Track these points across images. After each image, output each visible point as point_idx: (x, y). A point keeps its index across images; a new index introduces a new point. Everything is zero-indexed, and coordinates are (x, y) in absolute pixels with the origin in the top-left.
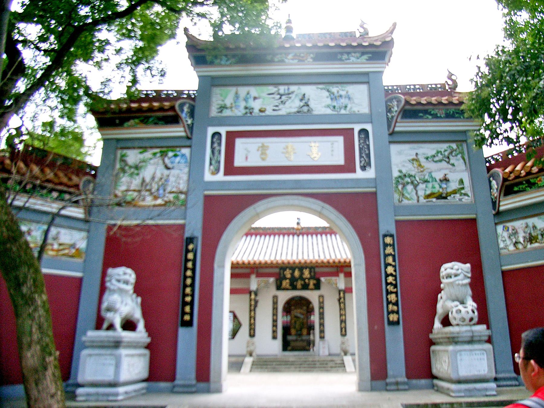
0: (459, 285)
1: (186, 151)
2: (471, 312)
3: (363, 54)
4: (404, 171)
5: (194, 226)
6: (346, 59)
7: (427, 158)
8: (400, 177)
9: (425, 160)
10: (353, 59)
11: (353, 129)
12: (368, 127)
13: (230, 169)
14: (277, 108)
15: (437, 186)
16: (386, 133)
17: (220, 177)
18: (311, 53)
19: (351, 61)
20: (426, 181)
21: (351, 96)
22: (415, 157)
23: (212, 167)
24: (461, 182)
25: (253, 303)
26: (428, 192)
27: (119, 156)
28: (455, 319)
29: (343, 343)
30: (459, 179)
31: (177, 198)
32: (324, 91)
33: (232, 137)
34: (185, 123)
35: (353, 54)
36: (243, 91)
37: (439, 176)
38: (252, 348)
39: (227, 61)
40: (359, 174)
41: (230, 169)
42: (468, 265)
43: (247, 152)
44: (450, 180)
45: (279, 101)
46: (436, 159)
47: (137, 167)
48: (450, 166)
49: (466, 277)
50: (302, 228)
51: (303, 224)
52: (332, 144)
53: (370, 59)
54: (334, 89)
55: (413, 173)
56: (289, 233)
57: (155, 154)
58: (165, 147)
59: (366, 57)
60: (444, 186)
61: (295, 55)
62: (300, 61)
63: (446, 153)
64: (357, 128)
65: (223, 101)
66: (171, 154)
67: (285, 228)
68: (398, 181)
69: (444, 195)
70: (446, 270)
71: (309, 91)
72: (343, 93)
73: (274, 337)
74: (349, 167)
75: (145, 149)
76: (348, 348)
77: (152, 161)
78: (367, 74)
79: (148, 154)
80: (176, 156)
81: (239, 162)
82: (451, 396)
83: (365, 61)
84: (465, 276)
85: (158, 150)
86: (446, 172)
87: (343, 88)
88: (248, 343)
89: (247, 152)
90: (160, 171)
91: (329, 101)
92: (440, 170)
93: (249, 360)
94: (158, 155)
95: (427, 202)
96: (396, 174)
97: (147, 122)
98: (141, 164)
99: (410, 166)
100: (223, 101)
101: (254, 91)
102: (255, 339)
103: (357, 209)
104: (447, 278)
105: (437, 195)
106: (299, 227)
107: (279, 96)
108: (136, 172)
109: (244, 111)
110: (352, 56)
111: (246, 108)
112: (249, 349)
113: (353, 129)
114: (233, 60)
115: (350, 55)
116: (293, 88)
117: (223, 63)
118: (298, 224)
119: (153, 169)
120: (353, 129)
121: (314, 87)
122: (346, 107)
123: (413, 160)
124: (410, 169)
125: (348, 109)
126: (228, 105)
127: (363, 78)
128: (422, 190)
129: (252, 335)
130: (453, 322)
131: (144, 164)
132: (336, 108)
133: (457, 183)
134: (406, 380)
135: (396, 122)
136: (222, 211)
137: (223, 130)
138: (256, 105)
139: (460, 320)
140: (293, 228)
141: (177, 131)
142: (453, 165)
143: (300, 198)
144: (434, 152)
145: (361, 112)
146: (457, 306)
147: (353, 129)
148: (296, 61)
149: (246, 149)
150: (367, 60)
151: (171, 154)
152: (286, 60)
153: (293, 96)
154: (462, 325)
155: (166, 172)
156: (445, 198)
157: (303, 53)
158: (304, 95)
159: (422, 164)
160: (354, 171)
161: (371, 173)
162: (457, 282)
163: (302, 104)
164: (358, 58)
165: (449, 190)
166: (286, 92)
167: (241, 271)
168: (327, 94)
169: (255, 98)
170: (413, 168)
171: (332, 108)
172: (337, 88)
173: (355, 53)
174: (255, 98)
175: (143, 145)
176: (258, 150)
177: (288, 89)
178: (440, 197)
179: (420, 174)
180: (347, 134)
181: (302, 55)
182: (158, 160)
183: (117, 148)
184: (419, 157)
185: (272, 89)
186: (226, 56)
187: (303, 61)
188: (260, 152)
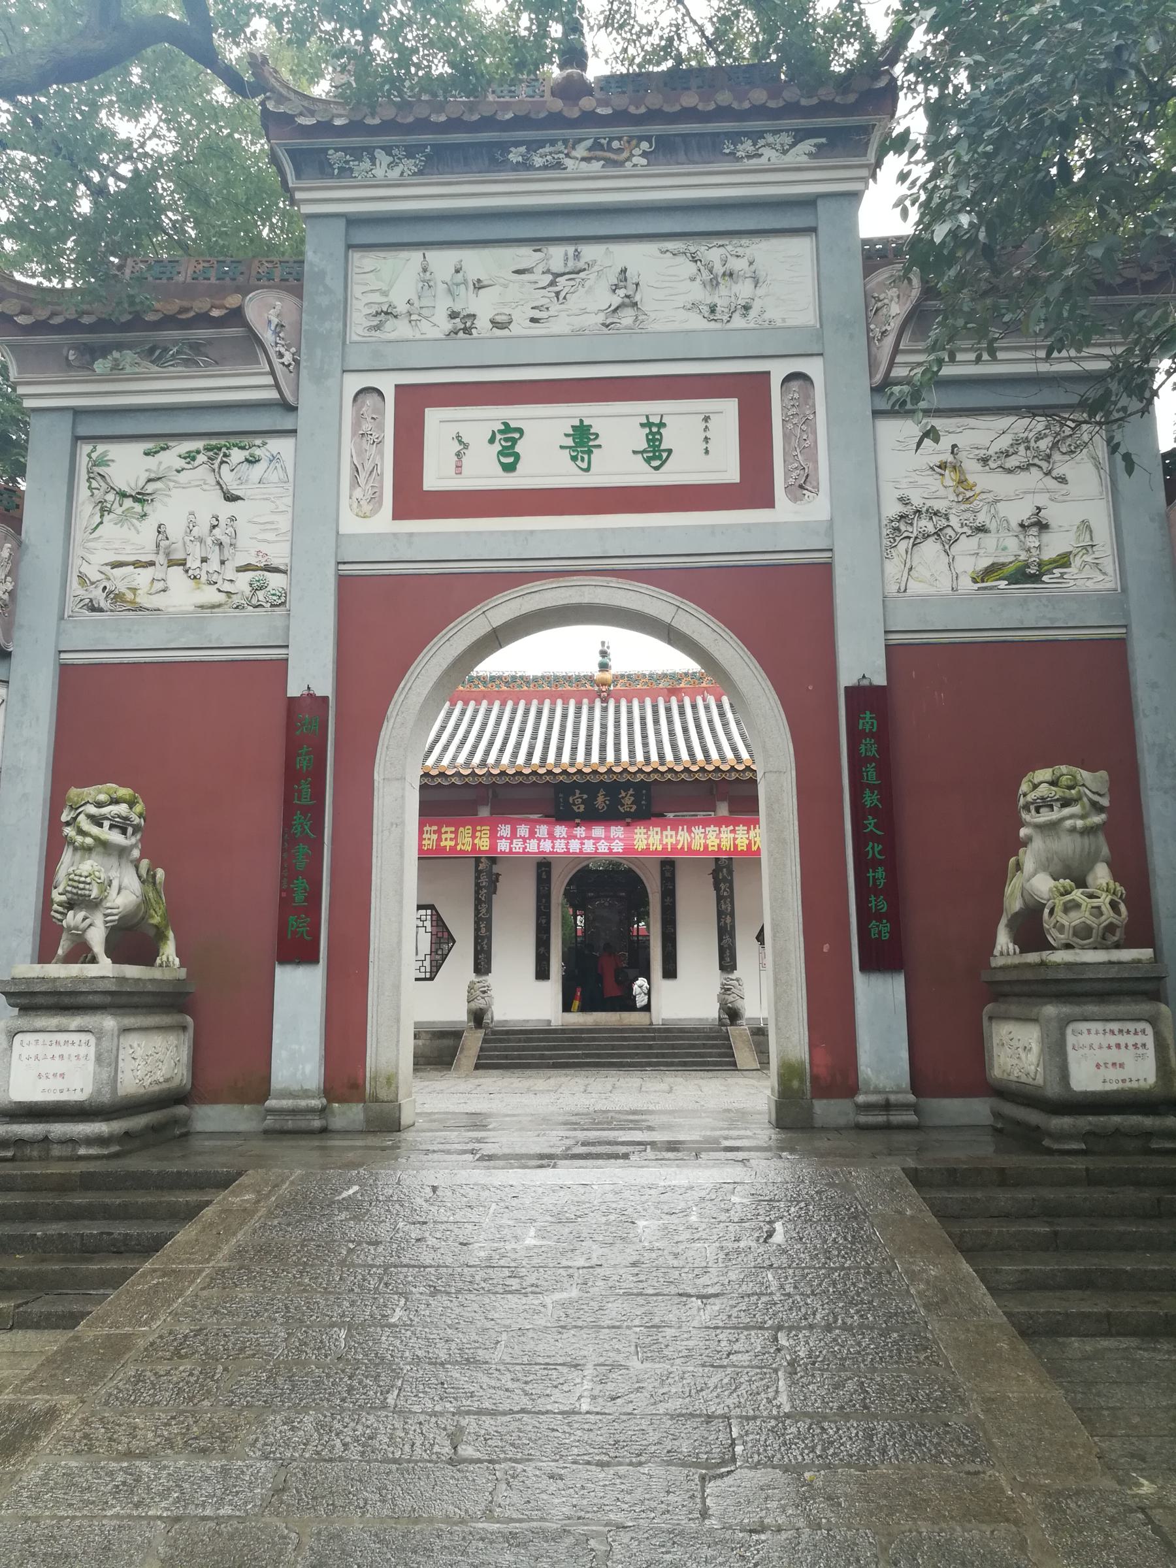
0: (1073, 830)
1: (282, 446)
2: (1106, 909)
3: (800, 136)
4: (917, 501)
5: (312, 672)
6: (749, 157)
7: (985, 461)
8: (902, 517)
9: (978, 466)
10: (767, 153)
11: (768, 373)
12: (813, 368)
13: (413, 500)
14: (543, 315)
15: (1012, 544)
16: (865, 385)
17: (383, 521)
18: (641, 139)
19: (764, 160)
20: (982, 529)
21: (761, 274)
22: (950, 458)
23: (358, 493)
24: (1086, 526)
25: (484, 881)
26: (984, 563)
27: (83, 462)
28: (1061, 928)
29: (726, 990)
30: (1078, 523)
31: (257, 587)
32: (681, 259)
33: (413, 403)
34: (276, 361)
35: (770, 139)
36: (442, 261)
37: (1022, 511)
38: (480, 1003)
39: (391, 166)
40: (785, 510)
41: (413, 500)
42: (1103, 774)
43: (458, 448)
44: (1053, 524)
45: (550, 293)
46: (1012, 462)
47: (140, 498)
48: (1050, 483)
49: (1097, 808)
50: (617, 678)
51: (618, 666)
52: (706, 419)
53: (820, 152)
54: (713, 254)
55: (938, 505)
56: (593, 677)
57: (190, 457)
58: (223, 434)
59: (807, 146)
60: (1032, 542)
61: (597, 146)
62: (610, 162)
63: (1044, 444)
64: (778, 371)
65: (385, 294)
66: (237, 455)
67: (568, 679)
68: (898, 529)
69: (1033, 570)
70: (1035, 786)
71: (639, 258)
72: (737, 265)
73: (542, 973)
74: (753, 489)
75: (163, 440)
76: (739, 1004)
77: (183, 477)
78: (809, 203)
79: (171, 458)
80: (252, 461)
81: (436, 476)
82: (1050, 1152)
83: (805, 158)
84: (1094, 804)
85: (199, 444)
86: (1041, 500)
87: (740, 251)
88: (471, 988)
89: (458, 448)
90: (210, 504)
91: (697, 292)
92: (1019, 497)
93: (473, 1042)
94: (201, 458)
95: (979, 589)
96: (892, 509)
97: (160, 357)
98: (150, 488)
99: (933, 483)
100: (385, 294)
101: (477, 262)
102: (490, 979)
103: (778, 610)
104: (111, 827)
105: (1010, 569)
106: (608, 676)
107: (550, 277)
108: (138, 507)
109: (447, 326)
110: (769, 145)
111: (453, 315)
112: (474, 1005)
113: (767, 374)
114: (409, 165)
115: (761, 142)
116: (590, 252)
117: (379, 172)
118: (604, 667)
119: (187, 499)
120: (767, 374)
121: (650, 249)
122: (747, 308)
123: (943, 466)
124: (935, 492)
125: (753, 313)
126: (402, 308)
127: (794, 215)
128: (972, 556)
129: (482, 964)
130: (1054, 937)
131: (158, 485)
132: (718, 309)
133: (1072, 535)
134: (911, 1098)
135: (896, 351)
136: (387, 618)
137: (387, 384)
138: (483, 307)
139: (1075, 934)
140: (590, 679)
141: (247, 384)
142: (1062, 480)
143: (614, 582)
144: (1005, 442)
145: (789, 323)
146: (1067, 893)
147: (768, 373)
148: (596, 166)
149: (459, 439)
150: (810, 155)
151: (237, 455)
152: (568, 162)
153: (591, 276)
154: (1083, 948)
155: (226, 510)
156: (1036, 578)
157: (620, 139)
158: (624, 271)
159: (971, 479)
160: (768, 502)
161: (817, 508)
162: (1068, 823)
163: (616, 300)
164: (785, 152)
165: (1049, 554)
166: (571, 264)
167: (446, 799)
168: (692, 268)
169: (479, 286)
170: (942, 492)
171: (706, 310)
172: (722, 250)
173: (776, 132)
174: (479, 286)
175: (155, 427)
176: (492, 441)
177: (577, 256)
178: (1023, 575)
179: (963, 507)
180: (751, 393)
181: (615, 144)
182: (201, 472)
183: (77, 439)
184: (962, 455)
185: (525, 256)
186: (388, 150)
187: (621, 164)
188: (497, 447)
